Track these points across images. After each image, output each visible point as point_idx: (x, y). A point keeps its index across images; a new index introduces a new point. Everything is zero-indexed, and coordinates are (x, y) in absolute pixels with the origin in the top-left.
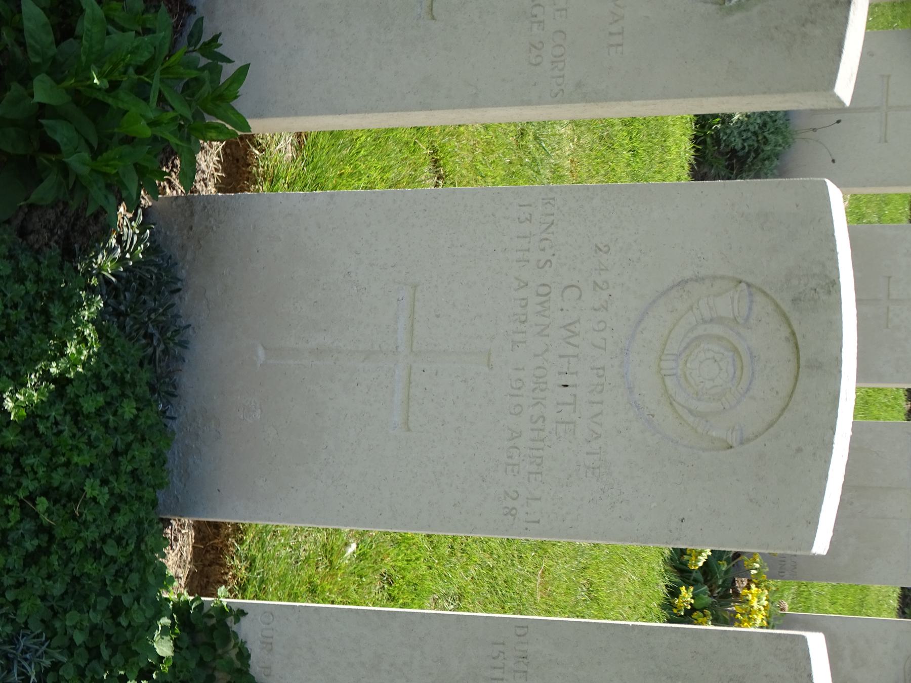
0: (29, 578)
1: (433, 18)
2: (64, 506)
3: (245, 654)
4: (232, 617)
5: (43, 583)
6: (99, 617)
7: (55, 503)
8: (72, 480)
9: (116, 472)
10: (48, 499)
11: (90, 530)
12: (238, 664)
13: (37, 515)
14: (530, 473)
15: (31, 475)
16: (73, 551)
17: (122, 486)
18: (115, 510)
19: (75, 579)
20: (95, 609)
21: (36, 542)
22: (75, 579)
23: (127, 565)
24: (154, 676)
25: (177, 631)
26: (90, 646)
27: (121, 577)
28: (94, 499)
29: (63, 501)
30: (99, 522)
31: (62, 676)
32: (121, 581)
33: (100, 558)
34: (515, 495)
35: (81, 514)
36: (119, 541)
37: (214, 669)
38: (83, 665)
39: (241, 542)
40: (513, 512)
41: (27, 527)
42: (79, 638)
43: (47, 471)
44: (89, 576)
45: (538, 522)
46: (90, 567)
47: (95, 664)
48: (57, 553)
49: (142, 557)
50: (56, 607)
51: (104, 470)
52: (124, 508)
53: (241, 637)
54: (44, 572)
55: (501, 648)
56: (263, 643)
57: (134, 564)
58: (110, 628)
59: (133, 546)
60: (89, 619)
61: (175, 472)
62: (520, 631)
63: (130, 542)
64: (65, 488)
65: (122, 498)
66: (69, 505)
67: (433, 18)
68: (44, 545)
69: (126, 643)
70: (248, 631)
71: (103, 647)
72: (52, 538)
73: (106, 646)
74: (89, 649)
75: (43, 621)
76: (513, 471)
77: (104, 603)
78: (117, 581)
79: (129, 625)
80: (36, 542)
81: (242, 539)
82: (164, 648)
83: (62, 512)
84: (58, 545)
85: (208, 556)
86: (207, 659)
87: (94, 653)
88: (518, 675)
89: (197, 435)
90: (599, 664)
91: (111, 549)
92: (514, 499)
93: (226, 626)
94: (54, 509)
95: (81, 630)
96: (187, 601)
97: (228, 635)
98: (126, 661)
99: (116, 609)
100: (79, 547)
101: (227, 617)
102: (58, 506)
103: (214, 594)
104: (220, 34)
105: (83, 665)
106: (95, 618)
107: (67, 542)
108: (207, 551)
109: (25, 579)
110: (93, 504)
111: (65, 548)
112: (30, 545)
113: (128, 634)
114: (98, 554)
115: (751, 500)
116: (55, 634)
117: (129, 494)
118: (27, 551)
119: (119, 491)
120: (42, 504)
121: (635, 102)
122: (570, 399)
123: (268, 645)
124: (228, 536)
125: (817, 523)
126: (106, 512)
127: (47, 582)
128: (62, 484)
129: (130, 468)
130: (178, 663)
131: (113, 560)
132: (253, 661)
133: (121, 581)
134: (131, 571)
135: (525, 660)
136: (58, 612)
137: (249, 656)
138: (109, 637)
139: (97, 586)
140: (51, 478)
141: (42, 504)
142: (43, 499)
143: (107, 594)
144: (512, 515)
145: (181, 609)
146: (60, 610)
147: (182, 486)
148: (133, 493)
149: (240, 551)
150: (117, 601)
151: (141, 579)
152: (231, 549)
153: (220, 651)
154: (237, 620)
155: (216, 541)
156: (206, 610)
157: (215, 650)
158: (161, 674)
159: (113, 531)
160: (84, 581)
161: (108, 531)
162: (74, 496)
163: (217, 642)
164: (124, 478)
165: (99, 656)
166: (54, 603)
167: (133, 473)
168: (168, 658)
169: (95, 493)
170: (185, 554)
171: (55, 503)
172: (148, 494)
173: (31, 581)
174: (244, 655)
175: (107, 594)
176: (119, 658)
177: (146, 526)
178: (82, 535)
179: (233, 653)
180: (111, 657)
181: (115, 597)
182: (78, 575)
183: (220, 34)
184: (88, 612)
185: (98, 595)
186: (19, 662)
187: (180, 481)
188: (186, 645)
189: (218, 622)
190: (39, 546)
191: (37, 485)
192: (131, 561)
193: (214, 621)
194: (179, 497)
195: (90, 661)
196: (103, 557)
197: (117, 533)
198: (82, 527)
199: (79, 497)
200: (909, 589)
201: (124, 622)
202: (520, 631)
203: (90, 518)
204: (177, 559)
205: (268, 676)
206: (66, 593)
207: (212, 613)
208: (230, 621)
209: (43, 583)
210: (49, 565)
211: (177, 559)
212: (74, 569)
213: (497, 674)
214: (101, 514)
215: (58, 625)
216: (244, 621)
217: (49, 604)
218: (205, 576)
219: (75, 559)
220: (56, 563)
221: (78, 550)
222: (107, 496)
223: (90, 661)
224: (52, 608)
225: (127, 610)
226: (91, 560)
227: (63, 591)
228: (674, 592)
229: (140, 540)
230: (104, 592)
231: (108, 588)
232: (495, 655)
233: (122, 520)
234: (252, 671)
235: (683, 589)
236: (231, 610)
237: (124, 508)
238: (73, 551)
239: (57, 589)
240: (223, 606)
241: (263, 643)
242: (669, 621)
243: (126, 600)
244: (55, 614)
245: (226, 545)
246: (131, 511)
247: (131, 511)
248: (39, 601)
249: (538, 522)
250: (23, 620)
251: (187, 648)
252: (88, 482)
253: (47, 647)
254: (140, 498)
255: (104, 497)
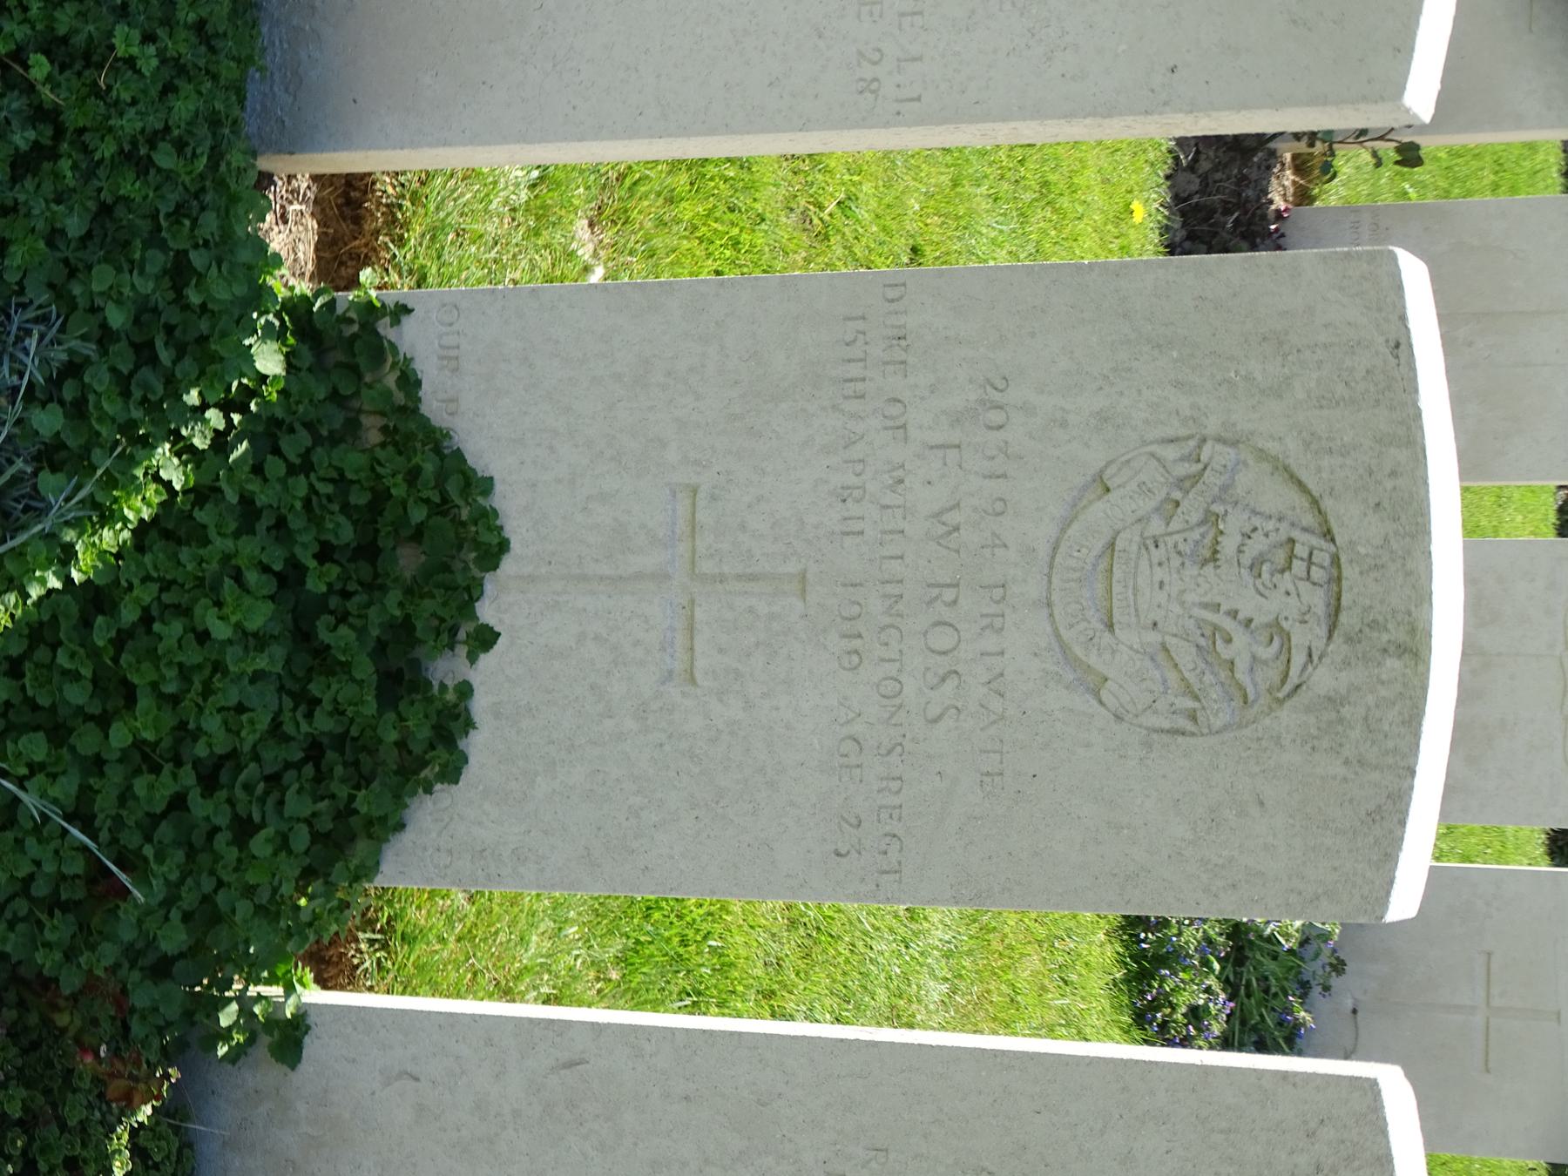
0: (22, 198)
2: (79, 74)
3: (412, 379)
4: (387, 320)
5: (48, 208)
6: (151, 285)
7: (63, 68)
8: (91, 28)
9: (168, 22)
10: (52, 62)
11: (126, 117)
12: (400, 398)
13: (30, 88)
14: (902, 15)
15: (17, 13)
16: (97, 157)
17: (182, 46)
18: (168, 89)
19: (105, 210)
20: (142, 272)
21: (31, 135)
22: (105, 210)
23: (196, 196)
24: (253, 407)
25: (291, 341)
26: (137, 340)
27: (187, 216)
28: (130, 62)
29: (78, 66)
30: (141, 107)
31: (90, 386)
32: (187, 223)
33: (147, 173)
34: (876, 57)
35: (109, 88)
36: (180, 146)
37: (360, 411)
38: (126, 372)
39: (401, 242)
40: (874, 86)
41: (15, 105)
42: (116, 318)
43: (45, 7)
44: (126, 200)
45: (919, 99)
46: (130, 186)
47: (146, 373)
48: (70, 156)
49: (221, 184)
50: (72, 261)
51: (148, 18)
52: (186, 87)
53: (404, 348)
54: (48, 188)
55: (860, 325)
56: (441, 358)
57: (208, 198)
58: (172, 316)
59: (204, 160)
60: (133, 286)
61: (277, 77)
62: (891, 293)
63: (198, 151)
64: (79, 40)
65: (181, 69)
66: (87, 73)
68: (47, 142)
69: (203, 340)
70: (415, 339)
71: (159, 343)
72: (59, 133)
73: (166, 344)
74: (137, 348)
75: (51, 286)
76: (871, 14)
77: (157, 261)
78: (179, 222)
79: (203, 306)
80: (31, 135)
81: (401, 238)
82: (269, 360)
83: (75, 83)
84: (71, 143)
85: (343, 271)
86: (346, 390)
87: (145, 353)
88: (890, 368)
89: (313, 8)
90: (1033, 335)
91: (165, 158)
92: (875, 63)
93: (377, 334)
94: (61, 78)
95: (119, 302)
96: (304, 297)
97: (379, 351)
98: (202, 373)
99: (180, 273)
100: (107, 149)
101: (378, 319)
102: (67, 73)
103: (354, 283)
105: (126, 372)
106: (146, 286)
107: (87, 137)
108: (342, 264)
109: (16, 200)
110: (130, 73)
111: (86, 150)
112: (22, 138)
113: (204, 325)
114: (143, 167)
115: (1294, 22)
116: (73, 307)
117: (195, 65)
118: (17, 149)
119: (175, 54)
120: (40, 67)
123: (451, 360)
124: (377, 232)
125: (1412, 50)
126: (154, 92)
127: (54, 207)
128: (75, 31)
129: (192, 17)
130: (294, 389)
131: (169, 176)
132: (426, 391)
133: (187, 223)
134: (203, 209)
135: (903, 343)
136: (77, 270)
137: (418, 383)
138: (169, 329)
139: (145, 226)
140: (52, 19)
141: (40, 67)
142: (42, 59)
143: (163, 246)
144: (873, 92)
145: (297, 309)
146: (80, 265)
147: (290, 100)
148: (202, 63)
149: (399, 258)
150: (181, 259)
151: (221, 228)
152: (383, 254)
153: (368, 378)
154: (396, 321)
155: (357, 243)
156: (340, 310)
157: (360, 377)
158: (264, 403)
159: (167, 129)
160: (120, 212)
161: (159, 126)
162: (95, 58)
163: (362, 361)
164: (182, 34)
165: (154, 360)
166: (68, 254)
167: (200, 26)
168: (275, 377)
169: (135, 51)
170: (301, 255)
171: (63, 68)
172: (228, 70)
173: (26, 203)
174: (410, 382)
175: (163, 246)
176: (188, 366)
177: (227, 131)
178: (112, 122)
179: (391, 380)
180: (174, 363)
181: (178, 252)
182: (109, 201)
184: (131, 272)
185: (147, 245)
186: (12, 356)
187: (286, 90)
188: (307, 365)
189: (362, 326)
190: (36, 145)
191: (29, 32)
192: (203, 190)
193: (356, 328)
194: (286, 119)
195: (137, 367)
196: (152, 172)
197: (176, 132)
198: (112, 110)
199: (105, 59)
200: (1564, 1166)
201: (195, 298)
202: (891, 293)
203: (126, 96)
204: (290, 240)
205: (451, 414)
206: (89, 235)
207: (353, 315)
208: (384, 327)
209: (48, 208)
210: (58, 176)
211: (290, 240)
212: (100, 190)
213: (855, 370)
214: (144, 92)
215: (77, 290)
216: (408, 323)
217: (59, 255)
218: (337, 262)
219: (101, 172)
220: (69, 174)
221: (107, 155)
222: (155, 62)
223: (137, 367)
224: (66, 261)
225: (200, 276)
226: (131, 175)
227: (83, 232)
229: (216, 156)
230: (155, 240)
231: (164, 234)
232: (848, 338)
233: (183, 107)
236: (383, 305)
237: (186, 87)
238: (97, 157)
239: (75, 225)
240: (371, 302)
241: (441, 358)
243: (197, 259)
244: (72, 273)
245: (374, 250)
246: (200, 93)
247: (200, 93)
248: (41, 245)
249: (919, 99)
250: (17, 278)
251: (310, 370)
252: (121, 30)
253: (59, 331)
254: (215, 77)
255: (149, 62)
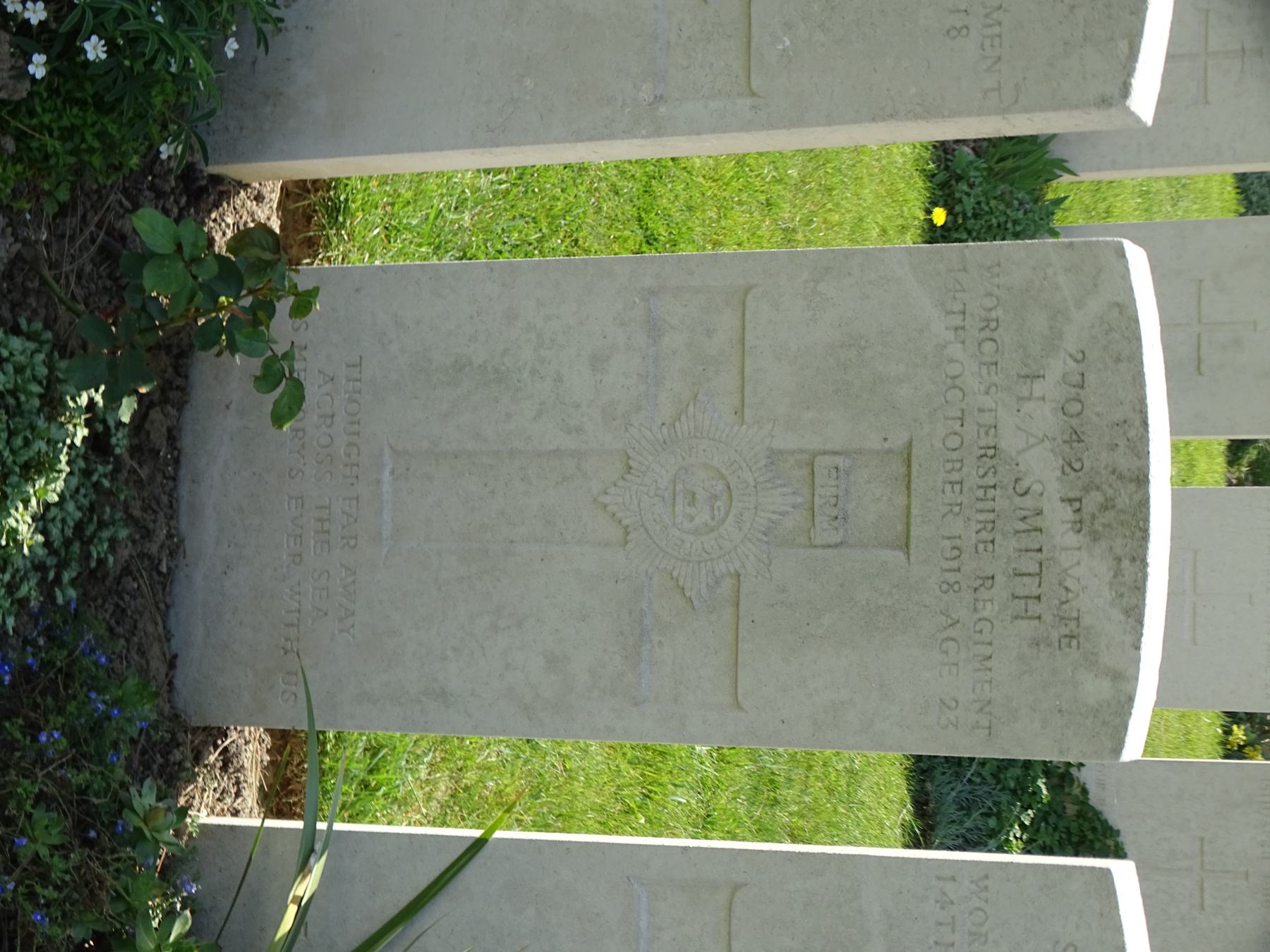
1: (1200, 374)
12: (1081, 798)
53: (1082, 781)
67: (1200, 374)
104: (317, 289)
121: (704, 136)
122: (1034, 568)
123: (1102, 785)
132: (1091, 796)
174: (1085, 791)
179: (1077, 791)
183: (317, 289)
208: (1073, 771)
215: (1002, 776)
228: (1228, 732)
234: (1091, 803)
235: (1235, 727)
242: (1226, 757)
